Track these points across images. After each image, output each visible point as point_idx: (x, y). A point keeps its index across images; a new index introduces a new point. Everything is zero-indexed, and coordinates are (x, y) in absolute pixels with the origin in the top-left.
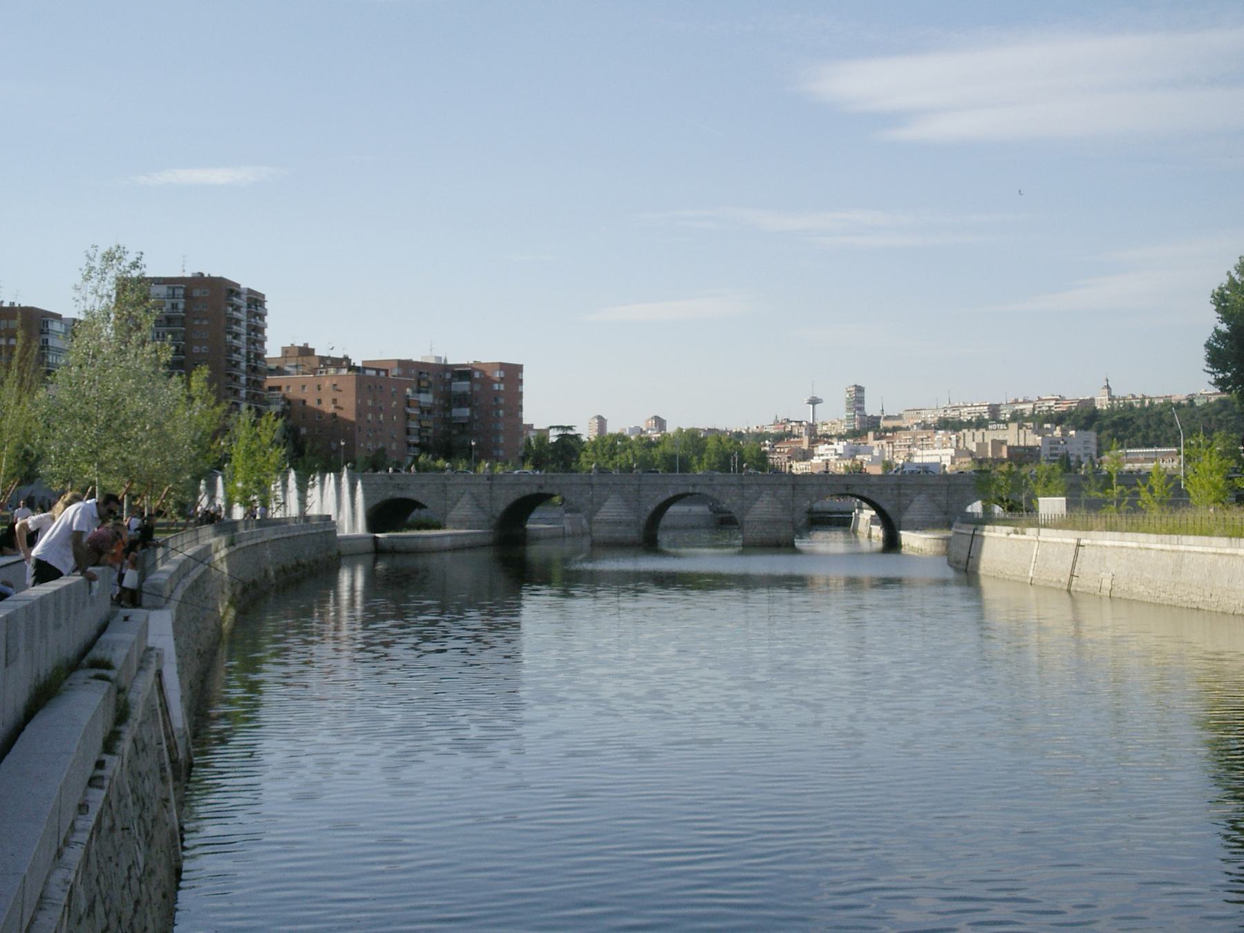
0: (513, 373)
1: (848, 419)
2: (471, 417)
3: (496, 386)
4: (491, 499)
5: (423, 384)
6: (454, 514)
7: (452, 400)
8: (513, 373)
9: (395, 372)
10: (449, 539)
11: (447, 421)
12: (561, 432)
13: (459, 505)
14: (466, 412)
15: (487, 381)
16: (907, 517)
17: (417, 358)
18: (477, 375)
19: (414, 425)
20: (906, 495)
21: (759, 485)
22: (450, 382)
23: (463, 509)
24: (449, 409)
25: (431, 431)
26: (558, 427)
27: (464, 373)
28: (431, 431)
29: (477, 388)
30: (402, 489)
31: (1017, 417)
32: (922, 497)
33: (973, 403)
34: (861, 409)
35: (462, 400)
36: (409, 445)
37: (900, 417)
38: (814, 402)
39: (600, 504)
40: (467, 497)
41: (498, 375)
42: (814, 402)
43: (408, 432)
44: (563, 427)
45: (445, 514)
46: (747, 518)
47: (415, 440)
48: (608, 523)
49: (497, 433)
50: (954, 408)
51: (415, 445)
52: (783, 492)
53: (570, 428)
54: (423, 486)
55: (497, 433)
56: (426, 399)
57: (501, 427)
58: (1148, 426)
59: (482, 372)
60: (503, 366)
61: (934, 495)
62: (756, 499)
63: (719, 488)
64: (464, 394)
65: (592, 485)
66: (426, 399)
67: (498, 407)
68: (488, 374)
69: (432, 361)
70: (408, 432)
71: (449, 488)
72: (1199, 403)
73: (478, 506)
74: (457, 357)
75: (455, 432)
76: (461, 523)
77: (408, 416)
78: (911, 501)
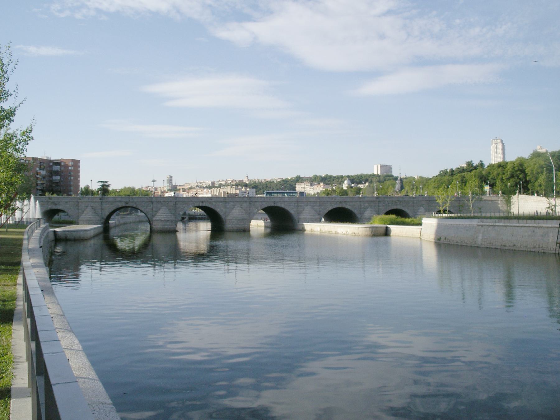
0: (76, 163)
1: (168, 186)
2: (60, 180)
3: (70, 168)
4: (102, 209)
5: (42, 167)
6: (83, 217)
7: (52, 173)
8: (76, 163)
9: (32, 161)
10: (92, 231)
11: (51, 181)
12: (103, 184)
13: (85, 212)
14: (58, 178)
15: (66, 166)
16: (302, 217)
17: (39, 157)
18: (63, 164)
19: (39, 182)
20: (301, 206)
21: (234, 202)
22: (52, 166)
23: (88, 214)
24: (51, 177)
25: (45, 185)
26: (101, 182)
27: (57, 163)
28: (45, 185)
29: (62, 169)
30: (55, 204)
31: (232, 186)
32: (309, 207)
33: (217, 178)
34: (171, 183)
35: (57, 173)
36: (37, 190)
37: (183, 185)
38: (154, 181)
39: (157, 212)
40: (89, 209)
41: (71, 164)
42: (154, 181)
43: (37, 185)
44: (103, 182)
45: (78, 217)
46: (229, 218)
47: (39, 188)
48: (161, 221)
49: (70, 186)
50: (201, 183)
51: (40, 190)
52: (244, 205)
53: (106, 182)
54: (66, 202)
55: (70, 186)
56: (43, 172)
57: (72, 183)
58: (263, 188)
59: (65, 163)
60: (73, 161)
61: (314, 206)
62: (232, 209)
63: (214, 203)
64: (57, 171)
65: (152, 202)
66: (43, 172)
67: (71, 176)
68: (67, 163)
69: (45, 158)
70: (37, 185)
71: (80, 204)
72: (275, 182)
73: (95, 213)
74: (55, 157)
75: (54, 185)
76: (89, 222)
77: (37, 178)
78: (304, 209)
